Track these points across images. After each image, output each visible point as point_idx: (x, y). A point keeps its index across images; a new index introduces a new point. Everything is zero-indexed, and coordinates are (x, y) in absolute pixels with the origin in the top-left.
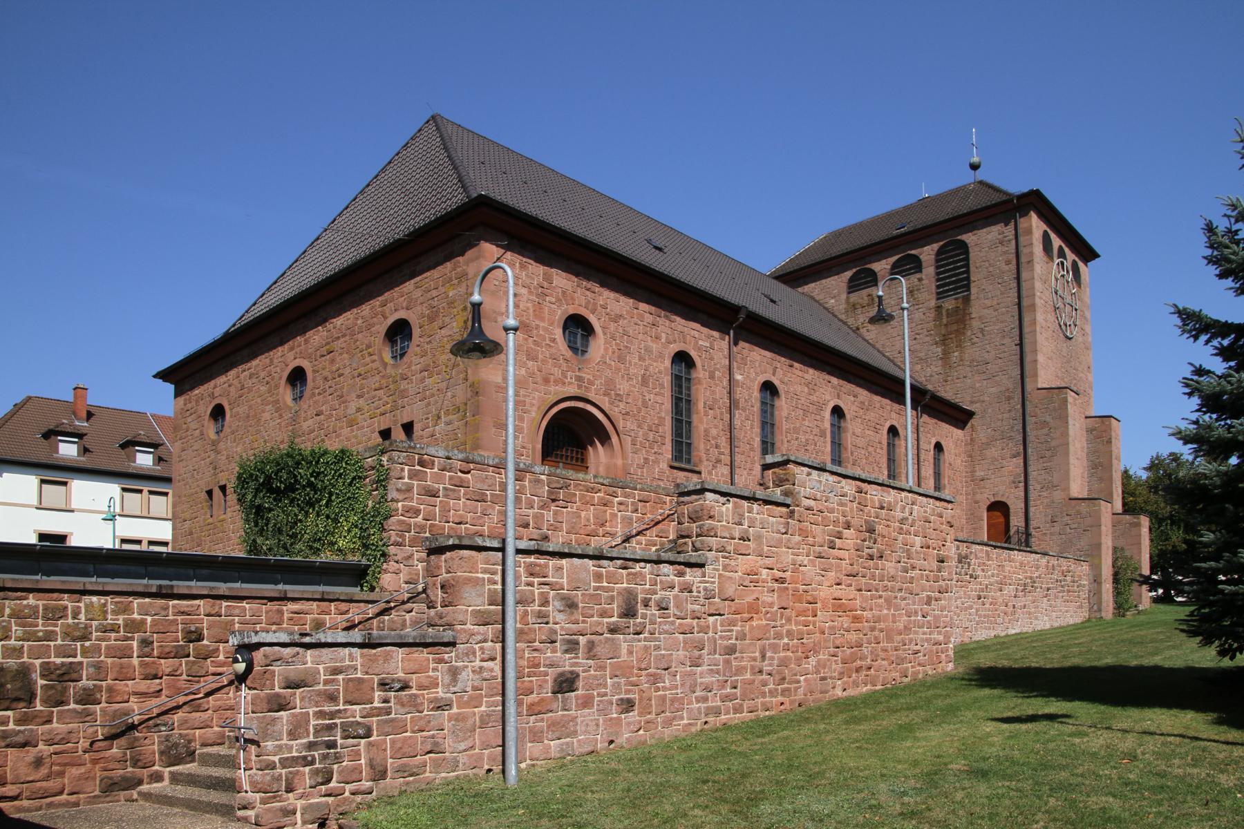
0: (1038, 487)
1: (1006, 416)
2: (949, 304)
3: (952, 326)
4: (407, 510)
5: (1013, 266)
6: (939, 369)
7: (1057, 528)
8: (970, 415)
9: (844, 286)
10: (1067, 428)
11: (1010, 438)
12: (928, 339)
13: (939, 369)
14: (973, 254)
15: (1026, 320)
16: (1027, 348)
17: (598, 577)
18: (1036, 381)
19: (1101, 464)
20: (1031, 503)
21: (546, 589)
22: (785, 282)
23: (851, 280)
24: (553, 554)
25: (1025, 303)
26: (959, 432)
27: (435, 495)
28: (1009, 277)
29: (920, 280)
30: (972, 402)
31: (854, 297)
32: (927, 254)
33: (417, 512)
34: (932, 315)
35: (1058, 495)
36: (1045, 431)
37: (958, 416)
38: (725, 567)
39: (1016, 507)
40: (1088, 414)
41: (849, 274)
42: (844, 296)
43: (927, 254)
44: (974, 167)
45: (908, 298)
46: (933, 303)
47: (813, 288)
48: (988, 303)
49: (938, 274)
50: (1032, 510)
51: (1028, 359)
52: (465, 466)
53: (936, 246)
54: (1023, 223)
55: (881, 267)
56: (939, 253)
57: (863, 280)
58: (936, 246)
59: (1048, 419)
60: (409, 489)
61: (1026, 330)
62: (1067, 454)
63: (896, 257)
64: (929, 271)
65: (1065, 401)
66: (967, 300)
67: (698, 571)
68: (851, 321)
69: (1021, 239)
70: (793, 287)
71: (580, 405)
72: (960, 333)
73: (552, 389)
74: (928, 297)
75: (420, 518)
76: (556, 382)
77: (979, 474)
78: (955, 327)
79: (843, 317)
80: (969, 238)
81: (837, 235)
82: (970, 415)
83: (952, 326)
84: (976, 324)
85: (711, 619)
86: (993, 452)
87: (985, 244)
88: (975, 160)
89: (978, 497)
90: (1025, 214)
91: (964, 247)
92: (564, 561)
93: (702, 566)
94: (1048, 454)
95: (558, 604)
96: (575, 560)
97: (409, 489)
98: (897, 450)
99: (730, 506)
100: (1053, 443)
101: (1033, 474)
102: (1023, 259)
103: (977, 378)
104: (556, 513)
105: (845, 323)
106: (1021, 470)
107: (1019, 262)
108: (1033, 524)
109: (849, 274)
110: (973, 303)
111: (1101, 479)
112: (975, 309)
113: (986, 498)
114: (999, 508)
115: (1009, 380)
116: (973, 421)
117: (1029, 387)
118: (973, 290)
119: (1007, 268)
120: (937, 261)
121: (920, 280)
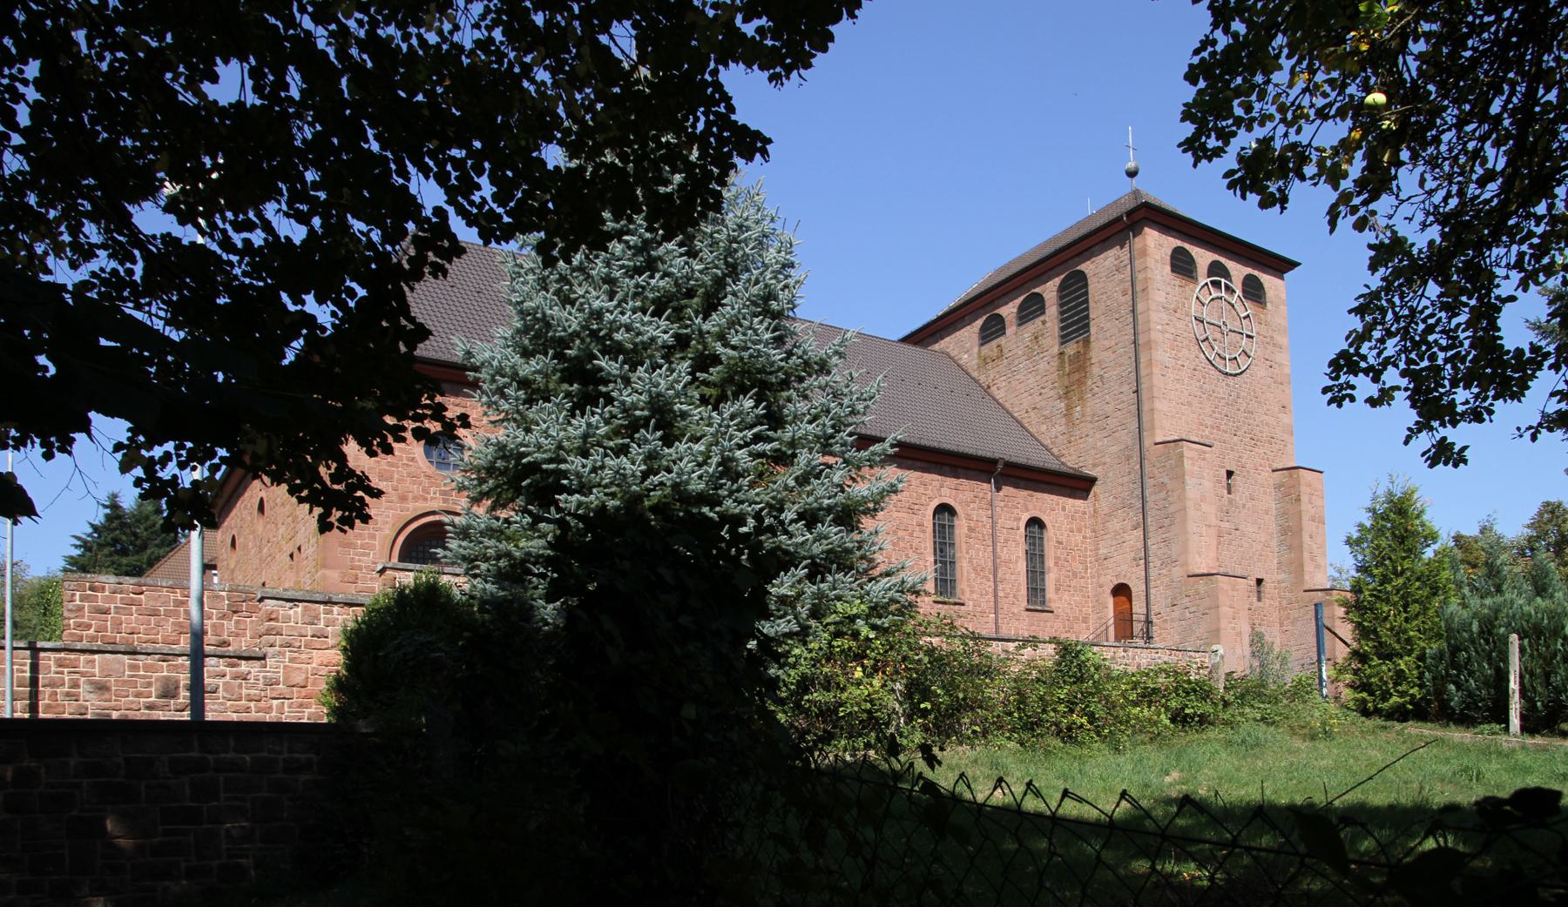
0: (1158, 563)
1: (1126, 479)
2: (1071, 348)
3: (1075, 374)
4: (79, 625)
5: (1129, 297)
6: (1062, 429)
7: (1176, 614)
8: (1091, 481)
9: (975, 338)
10: (1184, 489)
11: (1131, 506)
12: (1052, 393)
13: (1062, 429)
14: (1093, 287)
15: (1143, 360)
16: (1145, 395)
17: (134, 668)
18: (1153, 435)
19: (1289, 529)
20: (1152, 584)
21: (76, 676)
22: (915, 344)
23: (983, 328)
24: (83, 651)
25: (1142, 339)
26: (1079, 502)
27: (107, 612)
28: (1125, 310)
29: (1044, 323)
30: (1094, 465)
31: (986, 350)
32: (1049, 290)
33: (89, 627)
34: (1055, 363)
35: (1177, 572)
36: (1163, 495)
37: (1077, 485)
38: (292, 660)
39: (1137, 589)
40: (1276, 466)
41: (980, 322)
42: (976, 349)
43: (1049, 290)
44: (1132, 174)
45: (1031, 346)
46: (1056, 350)
47: (948, 344)
48: (1107, 343)
49: (1062, 313)
50: (1152, 591)
51: (1145, 407)
52: (137, 589)
53: (1057, 281)
54: (1138, 242)
55: (1009, 310)
56: (1062, 288)
57: (994, 329)
58: (1057, 281)
59: (1166, 480)
60: (80, 609)
61: (1143, 373)
62: (1184, 521)
63: (1022, 298)
64: (1052, 310)
65: (1181, 456)
66: (1087, 342)
67: (257, 663)
68: (982, 379)
69: (1137, 263)
70: (926, 347)
71: (437, 518)
72: (1081, 382)
73: (411, 505)
74: (1051, 342)
75: (92, 631)
76: (415, 499)
77: (1103, 551)
78: (1076, 376)
79: (975, 374)
80: (1087, 267)
81: (1001, 270)
82: (1091, 481)
83: (1075, 374)
84: (1095, 370)
85: (275, 702)
86: (1115, 525)
87: (1101, 269)
88: (1131, 165)
89: (1102, 579)
90: (1138, 233)
91: (1082, 276)
92: (96, 656)
93: (263, 658)
94: (1167, 522)
95: (88, 687)
96: (108, 656)
97: (80, 609)
98: (957, 532)
99: (299, 610)
100: (1172, 509)
101: (1152, 549)
102: (1139, 288)
103: (1098, 436)
104: (237, 622)
105: (977, 381)
106: (1140, 545)
107: (1135, 290)
108: (1154, 609)
109: (980, 322)
110: (1093, 345)
111: (1290, 548)
112: (1096, 353)
113: (1110, 582)
114: (1121, 591)
115: (1127, 437)
116: (1095, 489)
117: (1147, 443)
118: (1093, 330)
119: (1123, 299)
120: (1061, 298)
121: (1044, 323)
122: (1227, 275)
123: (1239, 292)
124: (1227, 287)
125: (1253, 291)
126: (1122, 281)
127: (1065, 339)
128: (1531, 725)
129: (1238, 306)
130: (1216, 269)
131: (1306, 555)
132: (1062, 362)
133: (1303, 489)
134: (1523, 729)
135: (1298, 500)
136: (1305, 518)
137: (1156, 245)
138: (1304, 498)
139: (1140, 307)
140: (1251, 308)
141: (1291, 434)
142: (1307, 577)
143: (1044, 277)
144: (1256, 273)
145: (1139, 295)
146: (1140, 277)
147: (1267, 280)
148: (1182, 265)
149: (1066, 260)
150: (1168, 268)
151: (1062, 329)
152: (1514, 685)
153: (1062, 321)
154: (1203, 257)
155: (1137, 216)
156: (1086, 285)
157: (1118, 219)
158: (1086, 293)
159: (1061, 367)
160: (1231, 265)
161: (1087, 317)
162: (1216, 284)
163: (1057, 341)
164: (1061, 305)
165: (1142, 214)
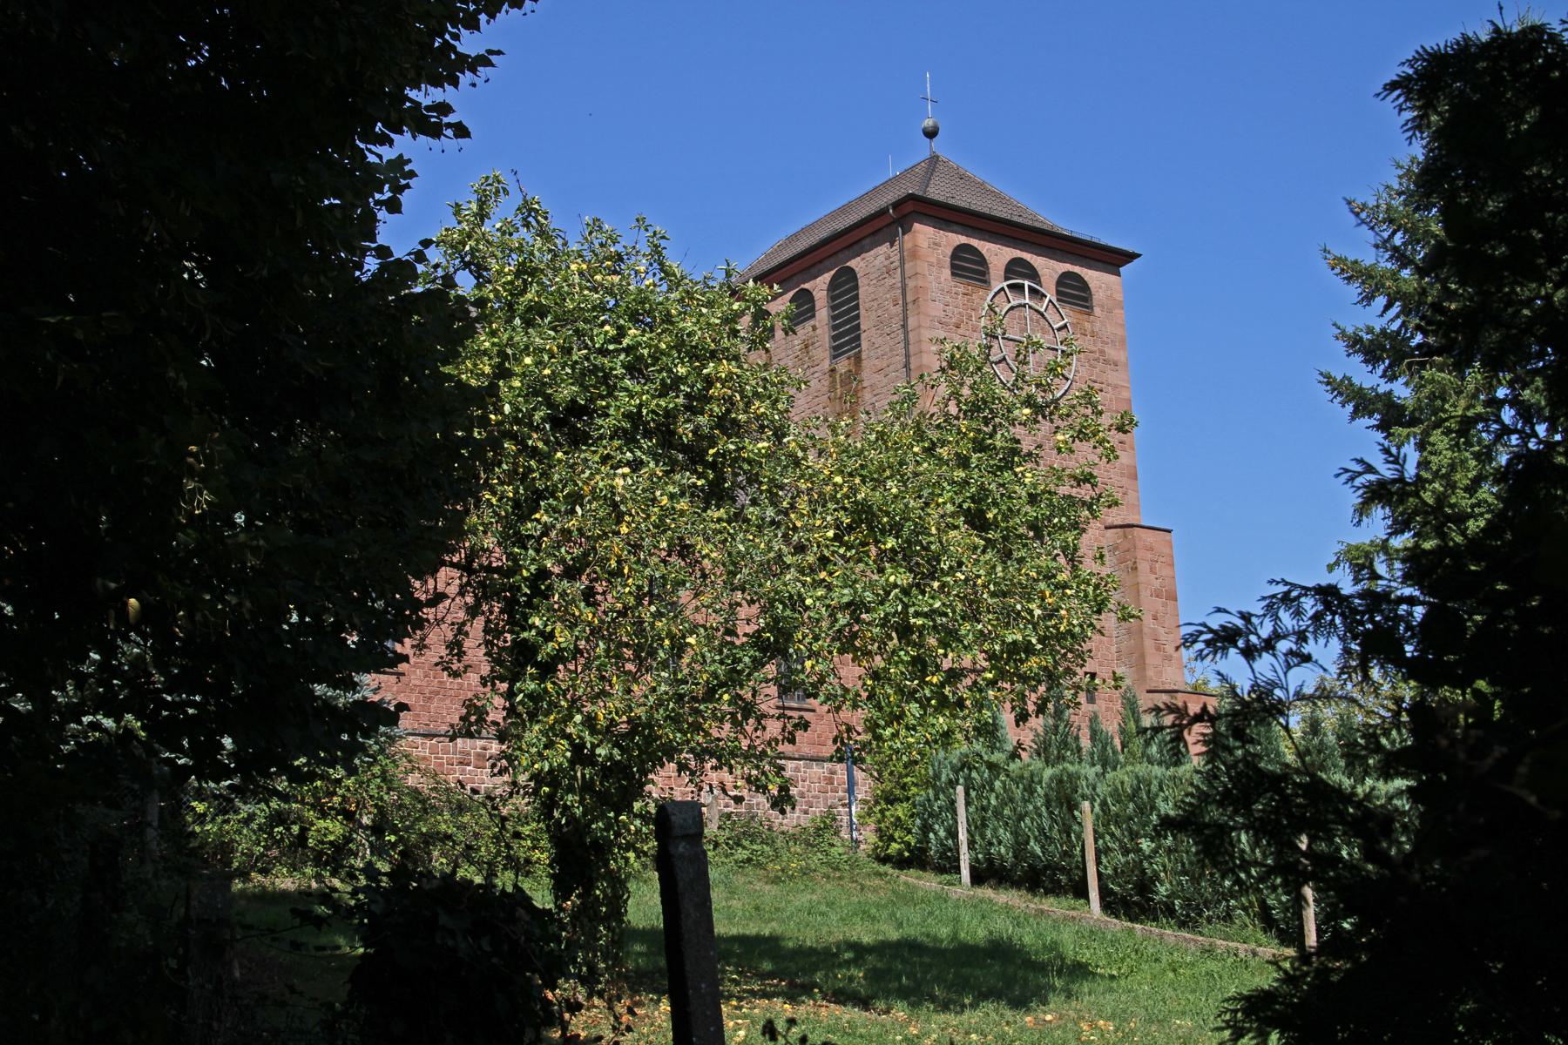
2: (843, 366)
5: (899, 309)
29: (814, 328)
32: (819, 286)
43: (819, 286)
44: (931, 134)
46: (826, 365)
49: (834, 318)
56: (833, 285)
64: (823, 314)
66: (858, 359)
74: (822, 353)
87: (869, 264)
88: (928, 123)
107: (907, 301)
110: (864, 363)
112: (868, 375)
118: (864, 344)
119: (894, 310)
120: (833, 298)
121: (814, 328)
122: (1033, 275)
123: (1051, 295)
124: (1033, 291)
125: (1074, 293)
126: (892, 287)
127: (837, 352)
128: (978, 878)
129: (1051, 315)
130: (1015, 268)
131: (1148, 644)
132: (833, 382)
133: (1140, 554)
134: (973, 883)
135: (1135, 569)
136: (1145, 594)
137: (932, 244)
138: (1143, 567)
139: (911, 322)
140: (1069, 315)
141: (1135, 477)
142: (1150, 673)
143: (814, 271)
144: (1076, 269)
145: (910, 306)
146: (911, 284)
147: (1092, 276)
148: (968, 266)
149: (835, 250)
150: (947, 272)
151: (835, 338)
152: (963, 836)
153: (835, 328)
154: (998, 255)
155: (909, 207)
156: (856, 287)
157: (882, 213)
158: (856, 297)
159: (832, 388)
160: (1038, 261)
161: (858, 327)
162: (1017, 288)
163: (827, 354)
164: (833, 308)
165: (909, 207)
